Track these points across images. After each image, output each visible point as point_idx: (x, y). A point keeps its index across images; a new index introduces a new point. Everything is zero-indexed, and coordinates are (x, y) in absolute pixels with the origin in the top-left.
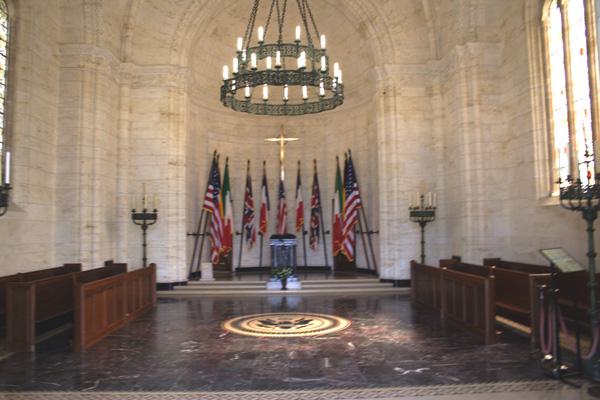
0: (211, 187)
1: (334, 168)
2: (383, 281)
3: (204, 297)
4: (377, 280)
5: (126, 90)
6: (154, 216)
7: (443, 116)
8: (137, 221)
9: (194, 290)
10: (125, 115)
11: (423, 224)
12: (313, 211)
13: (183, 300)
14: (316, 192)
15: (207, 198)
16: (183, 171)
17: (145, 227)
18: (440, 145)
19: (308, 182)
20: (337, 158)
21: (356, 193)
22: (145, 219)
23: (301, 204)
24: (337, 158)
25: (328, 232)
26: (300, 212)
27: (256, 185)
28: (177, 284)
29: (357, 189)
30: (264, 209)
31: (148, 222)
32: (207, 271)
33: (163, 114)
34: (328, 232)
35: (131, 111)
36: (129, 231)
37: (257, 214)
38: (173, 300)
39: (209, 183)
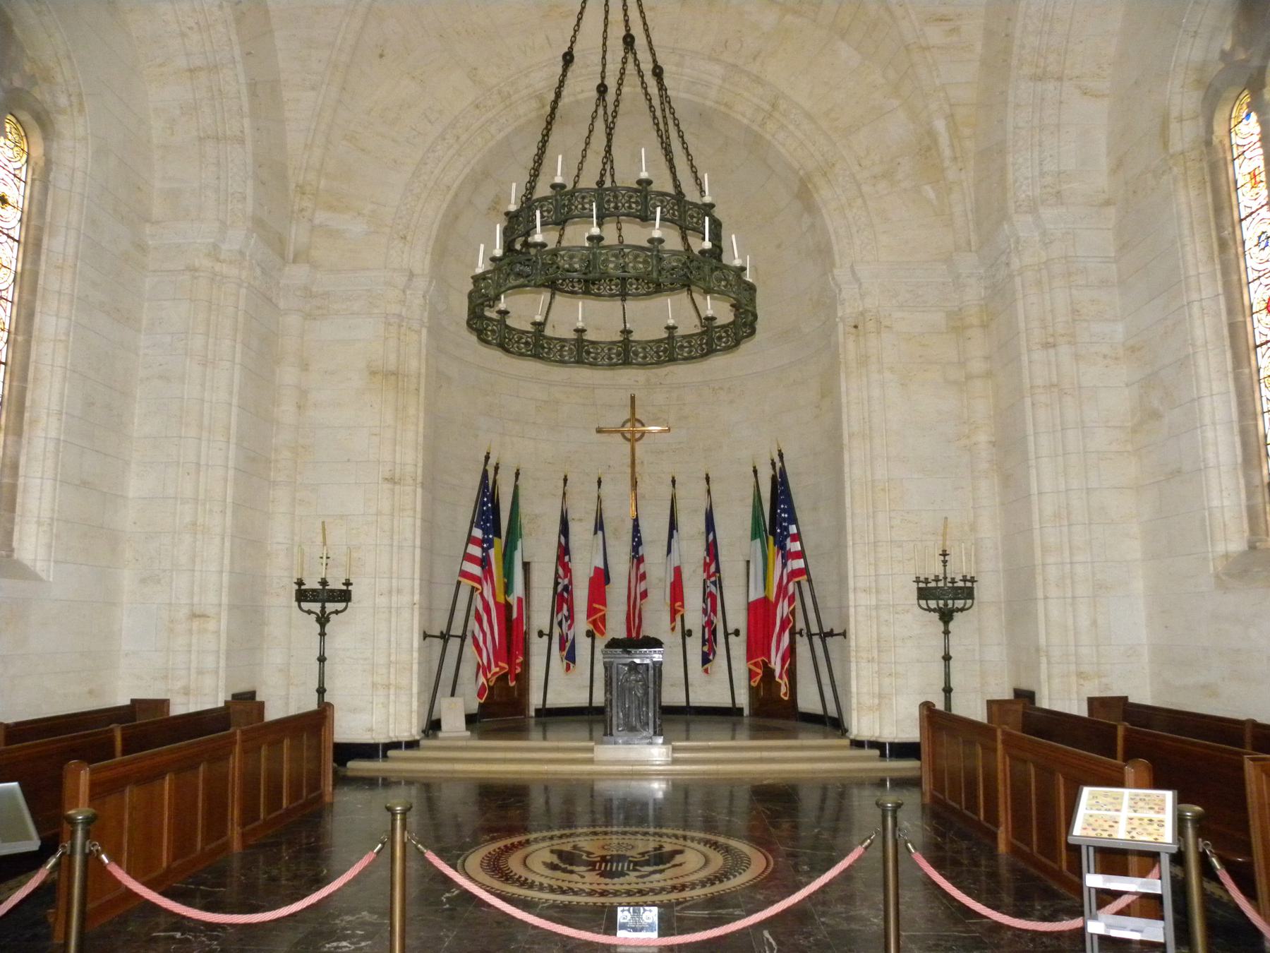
0: (478, 533)
2: (858, 744)
3: (452, 779)
6: (344, 596)
8: (305, 605)
11: (946, 616)
13: (410, 782)
15: (468, 557)
19: (691, 525)
22: (324, 599)
28: (396, 745)
31: (330, 607)
35: (305, 367)
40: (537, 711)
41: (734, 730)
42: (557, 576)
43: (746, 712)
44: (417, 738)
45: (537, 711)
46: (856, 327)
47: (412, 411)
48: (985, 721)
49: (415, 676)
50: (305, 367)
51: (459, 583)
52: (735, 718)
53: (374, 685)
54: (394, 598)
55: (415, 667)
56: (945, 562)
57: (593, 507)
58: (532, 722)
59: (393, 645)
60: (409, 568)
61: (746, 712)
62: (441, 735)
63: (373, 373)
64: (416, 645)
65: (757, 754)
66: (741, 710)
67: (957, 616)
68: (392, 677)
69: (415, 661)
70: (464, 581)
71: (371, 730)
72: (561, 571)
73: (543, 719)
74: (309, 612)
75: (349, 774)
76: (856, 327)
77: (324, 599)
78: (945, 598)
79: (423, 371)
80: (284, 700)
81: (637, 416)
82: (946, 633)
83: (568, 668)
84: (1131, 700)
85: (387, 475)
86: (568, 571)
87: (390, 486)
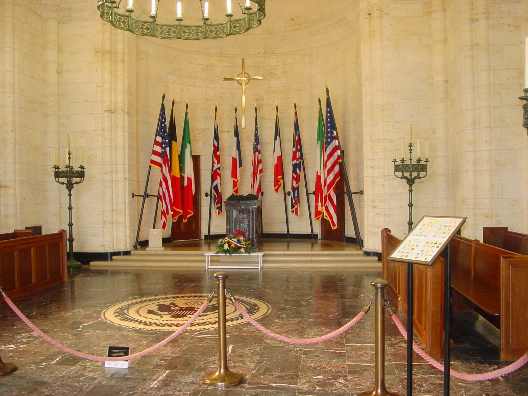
0: (159, 139)
1: (317, 115)
2: (368, 254)
3: (155, 271)
4: (361, 252)
5: (52, 25)
6: (81, 174)
7: (445, 40)
8: (61, 180)
9: (138, 261)
10: (52, 55)
11: (411, 182)
12: (295, 166)
13: (126, 273)
14: (298, 143)
15: (155, 153)
16: (122, 120)
17: (70, 186)
18: (440, 78)
19: (288, 133)
20: (320, 101)
21: (336, 143)
22: (71, 176)
23: (280, 159)
24: (320, 101)
25: (289, 194)
26: (279, 169)
27: (228, 141)
28: (118, 254)
29: (336, 138)
30: (237, 164)
31: (74, 180)
32: (155, 237)
33: (97, 52)
34: (289, 194)
35: (60, 50)
36: (56, 189)
37: (227, 172)
38: (115, 273)
39: (157, 134)
40: (205, 236)
41: (209, 246)
42: (213, 163)
43: (319, 237)
44: (129, 250)
45: (205, 236)
46: (370, 14)
47: (120, 73)
48: (482, 241)
49: (127, 217)
50: (60, 50)
51: (150, 166)
52: (313, 240)
53: (104, 222)
54: (114, 175)
55: (127, 212)
56: (411, 150)
57: (234, 124)
58: (203, 241)
59: (114, 201)
60: (121, 158)
61: (319, 237)
62: (147, 249)
63: (97, 52)
64: (127, 200)
65: (309, 258)
66: (317, 236)
67: (417, 180)
68: (114, 217)
69: (127, 209)
70: (153, 166)
71: (103, 245)
72: (216, 161)
73: (209, 241)
74: (63, 183)
75: (91, 268)
76: (370, 14)
77: (71, 176)
78: (412, 171)
79: (126, 50)
80: (51, 228)
81: (246, 71)
82: (411, 191)
83: (219, 213)
84: (509, 230)
85: (107, 109)
86: (218, 158)
87: (109, 114)
